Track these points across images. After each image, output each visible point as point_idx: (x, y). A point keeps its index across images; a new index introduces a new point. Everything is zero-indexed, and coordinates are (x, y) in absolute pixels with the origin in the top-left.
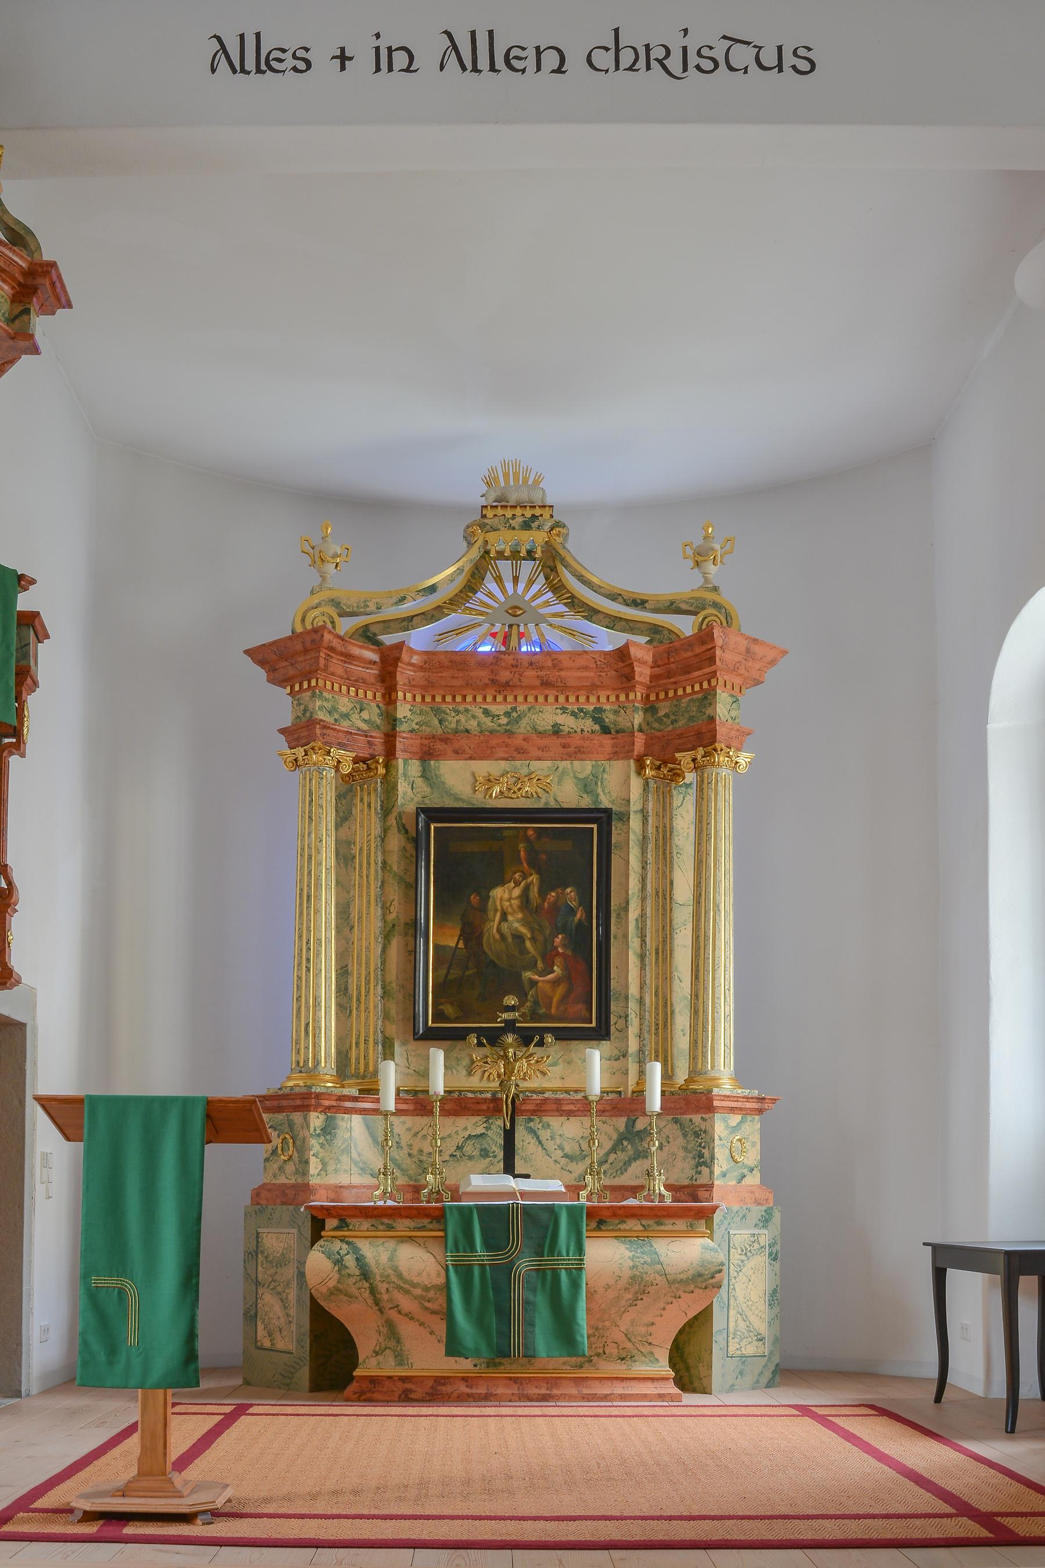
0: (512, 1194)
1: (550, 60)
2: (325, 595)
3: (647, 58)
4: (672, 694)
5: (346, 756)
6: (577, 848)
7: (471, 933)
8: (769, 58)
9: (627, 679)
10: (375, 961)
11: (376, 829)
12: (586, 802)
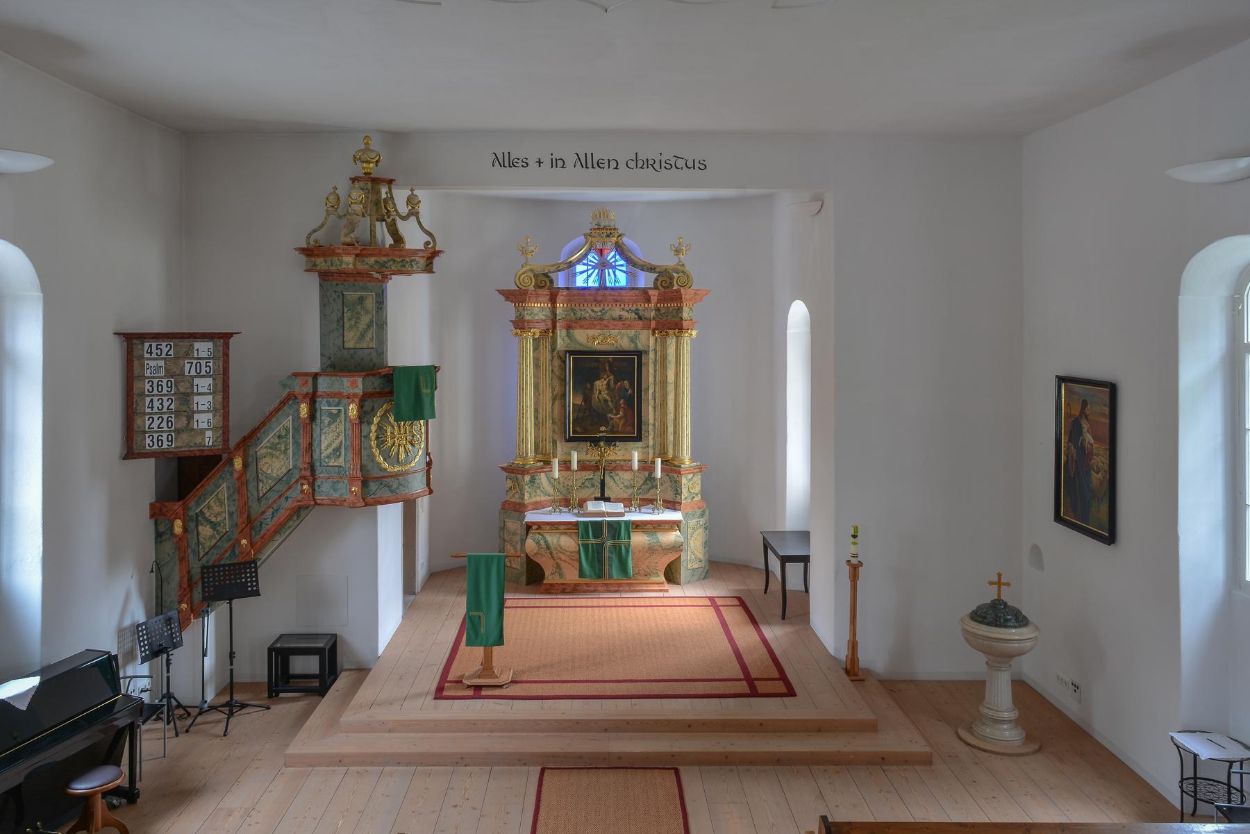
0: (602, 514)
1: (613, 164)
2: (528, 267)
3: (648, 164)
4: (665, 303)
5: (537, 332)
6: (627, 366)
7: (587, 399)
8: (690, 164)
9: (648, 300)
10: (549, 410)
11: (549, 357)
12: (631, 347)
